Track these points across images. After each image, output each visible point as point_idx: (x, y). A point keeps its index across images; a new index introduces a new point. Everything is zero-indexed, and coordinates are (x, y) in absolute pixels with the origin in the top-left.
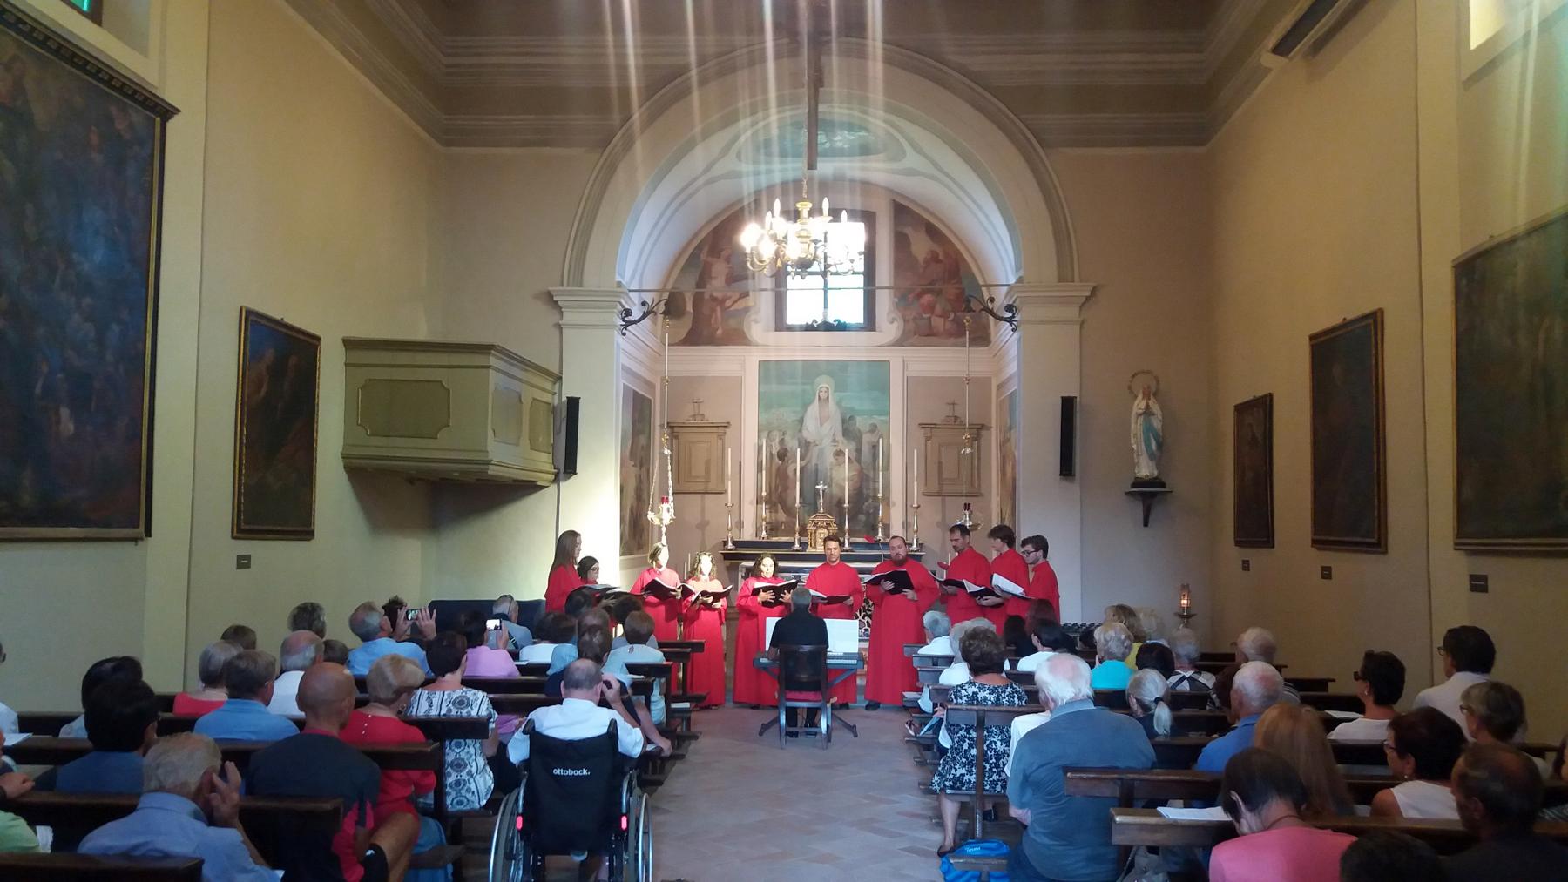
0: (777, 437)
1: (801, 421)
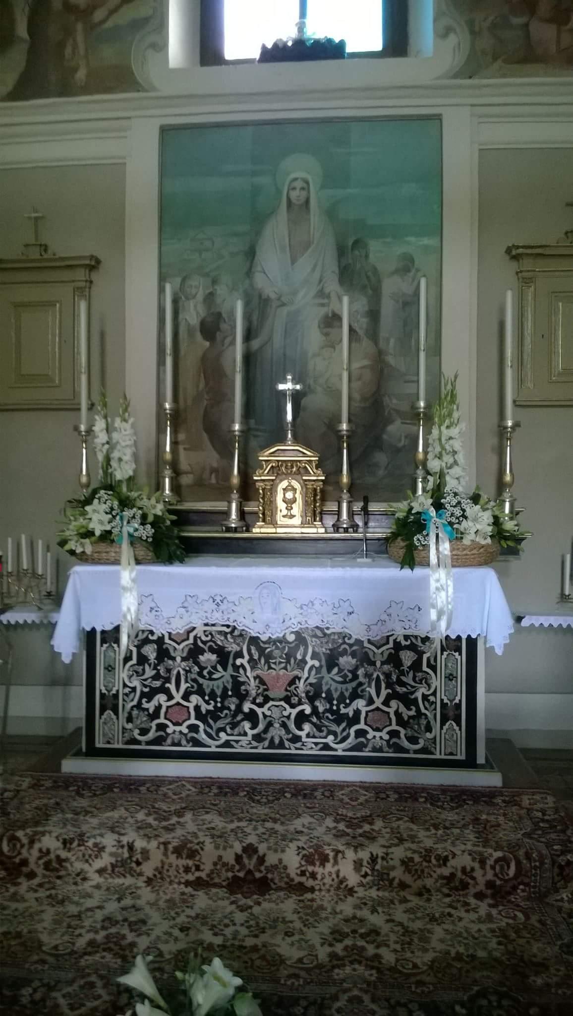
0: (198, 286)
1: (251, 254)
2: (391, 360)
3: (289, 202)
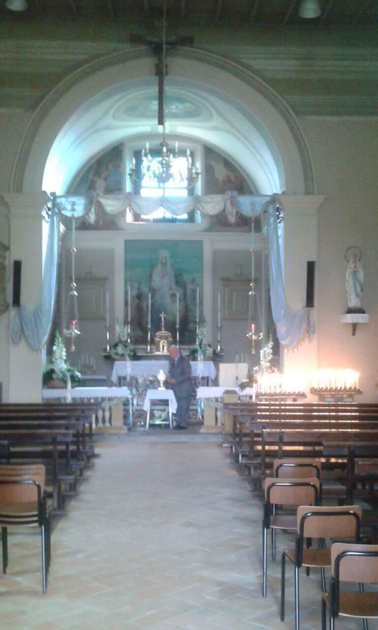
1: (150, 276)
2: (190, 306)
3: (162, 263)
